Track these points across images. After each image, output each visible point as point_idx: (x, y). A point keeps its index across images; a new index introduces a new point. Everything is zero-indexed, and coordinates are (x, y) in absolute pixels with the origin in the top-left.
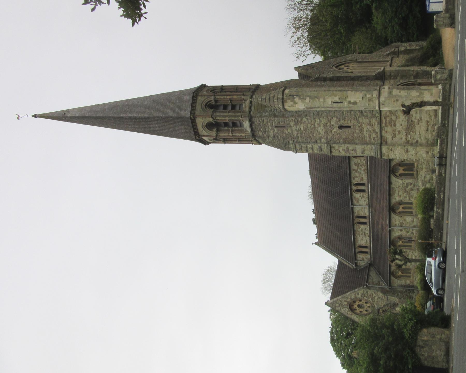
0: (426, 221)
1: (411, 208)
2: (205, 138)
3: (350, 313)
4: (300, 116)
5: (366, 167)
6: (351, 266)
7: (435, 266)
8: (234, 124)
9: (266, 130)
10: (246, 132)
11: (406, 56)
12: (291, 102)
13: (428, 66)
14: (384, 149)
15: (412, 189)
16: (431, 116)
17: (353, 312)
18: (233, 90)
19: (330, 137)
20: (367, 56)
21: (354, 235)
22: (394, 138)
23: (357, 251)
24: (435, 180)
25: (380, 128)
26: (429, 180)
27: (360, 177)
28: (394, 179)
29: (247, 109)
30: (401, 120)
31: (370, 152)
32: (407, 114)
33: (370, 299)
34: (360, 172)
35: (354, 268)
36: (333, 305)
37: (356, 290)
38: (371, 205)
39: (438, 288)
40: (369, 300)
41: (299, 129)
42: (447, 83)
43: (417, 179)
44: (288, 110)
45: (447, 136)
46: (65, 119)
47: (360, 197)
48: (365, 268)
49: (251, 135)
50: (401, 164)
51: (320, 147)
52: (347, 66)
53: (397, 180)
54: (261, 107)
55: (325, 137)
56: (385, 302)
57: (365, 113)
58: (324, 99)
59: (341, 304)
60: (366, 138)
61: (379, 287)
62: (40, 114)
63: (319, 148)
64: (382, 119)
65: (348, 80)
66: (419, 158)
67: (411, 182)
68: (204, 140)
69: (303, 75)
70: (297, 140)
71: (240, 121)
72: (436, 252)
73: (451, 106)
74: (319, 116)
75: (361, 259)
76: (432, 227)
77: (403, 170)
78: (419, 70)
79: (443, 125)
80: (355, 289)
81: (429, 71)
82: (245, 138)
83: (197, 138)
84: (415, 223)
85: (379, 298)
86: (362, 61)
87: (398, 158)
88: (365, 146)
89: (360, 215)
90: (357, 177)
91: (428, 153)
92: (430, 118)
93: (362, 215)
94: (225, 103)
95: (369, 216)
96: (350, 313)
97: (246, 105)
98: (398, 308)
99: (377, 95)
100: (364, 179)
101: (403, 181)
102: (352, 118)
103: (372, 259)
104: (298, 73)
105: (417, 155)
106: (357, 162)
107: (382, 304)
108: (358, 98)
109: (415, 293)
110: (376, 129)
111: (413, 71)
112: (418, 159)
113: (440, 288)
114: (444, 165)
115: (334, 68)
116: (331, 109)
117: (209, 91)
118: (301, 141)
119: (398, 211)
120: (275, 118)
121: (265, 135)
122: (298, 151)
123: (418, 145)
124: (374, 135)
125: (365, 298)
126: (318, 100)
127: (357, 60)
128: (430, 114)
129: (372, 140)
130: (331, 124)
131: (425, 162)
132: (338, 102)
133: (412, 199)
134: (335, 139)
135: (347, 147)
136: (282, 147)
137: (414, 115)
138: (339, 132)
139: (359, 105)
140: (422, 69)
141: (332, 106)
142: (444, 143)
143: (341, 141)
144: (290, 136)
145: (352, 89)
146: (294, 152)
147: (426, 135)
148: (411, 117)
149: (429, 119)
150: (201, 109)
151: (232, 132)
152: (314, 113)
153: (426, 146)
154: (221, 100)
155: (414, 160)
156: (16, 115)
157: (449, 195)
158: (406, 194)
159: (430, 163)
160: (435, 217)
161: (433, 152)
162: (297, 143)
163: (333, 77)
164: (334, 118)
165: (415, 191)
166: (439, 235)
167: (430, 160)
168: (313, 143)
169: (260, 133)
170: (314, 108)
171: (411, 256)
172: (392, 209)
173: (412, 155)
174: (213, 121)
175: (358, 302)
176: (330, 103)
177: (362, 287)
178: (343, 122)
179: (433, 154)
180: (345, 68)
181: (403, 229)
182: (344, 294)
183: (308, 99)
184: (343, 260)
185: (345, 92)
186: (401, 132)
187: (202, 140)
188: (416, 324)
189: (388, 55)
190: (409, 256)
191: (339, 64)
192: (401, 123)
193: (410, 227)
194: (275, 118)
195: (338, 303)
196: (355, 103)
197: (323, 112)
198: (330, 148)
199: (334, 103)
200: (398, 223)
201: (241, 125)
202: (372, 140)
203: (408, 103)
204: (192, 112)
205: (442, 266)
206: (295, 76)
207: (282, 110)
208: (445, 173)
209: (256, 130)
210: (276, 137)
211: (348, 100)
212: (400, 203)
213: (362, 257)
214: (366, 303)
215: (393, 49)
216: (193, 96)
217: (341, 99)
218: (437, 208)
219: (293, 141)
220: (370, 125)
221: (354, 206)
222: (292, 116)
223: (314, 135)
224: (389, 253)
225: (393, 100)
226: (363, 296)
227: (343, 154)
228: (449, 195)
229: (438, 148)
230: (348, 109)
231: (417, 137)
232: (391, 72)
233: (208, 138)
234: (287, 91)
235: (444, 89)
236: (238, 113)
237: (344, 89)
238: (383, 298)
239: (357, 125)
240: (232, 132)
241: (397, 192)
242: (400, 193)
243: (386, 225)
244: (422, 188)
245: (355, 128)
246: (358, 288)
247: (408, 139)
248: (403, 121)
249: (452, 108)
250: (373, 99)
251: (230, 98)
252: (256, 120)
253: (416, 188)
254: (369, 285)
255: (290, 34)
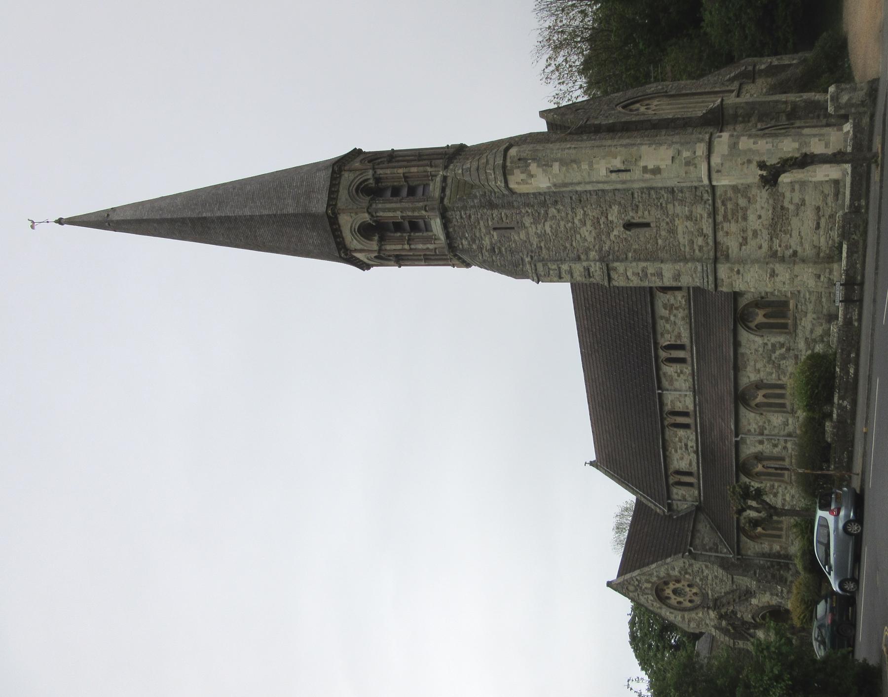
0: (814, 426)
1: (782, 396)
2: (360, 256)
3: (657, 604)
4: (544, 204)
5: (687, 311)
6: (660, 509)
7: (836, 528)
8: (414, 226)
9: (475, 236)
10: (436, 242)
11: (769, 80)
12: (522, 173)
13: (820, 92)
14: (723, 271)
15: (783, 357)
16: (826, 197)
17: (664, 604)
18: (413, 157)
19: (606, 248)
20: (685, 84)
21: (665, 449)
22: (744, 247)
23: (671, 480)
24: (836, 335)
25: (712, 225)
26: (822, 336)
27: (676, 333)
28: (745, 336)
29: (437, 194)
30: (758, 206)
31: (693, 278)
32: (771, 186)
33: (698, 580)
34: (674, 322)
35: (666, 514)
36: (623, 588)
37: (669, 560)
38: (698, 388)
39: (842, 578)
40: (696, 582)
41: (543, 231)
42: (865, 113)
43: (796, 335)
44: (518, 191)
45: (865, 232)
46: (109, 225)
47: (676, 372)
48: (687, 515)
49: (447, 248)
50: (761, 302)
51: (587, 270)
52: (647, 105)
53: (752, 337)
54: (465, 189)
55: (597, 247)
56: (728, 587)
57: (680, 194)
58: (591, 164)
59: (638, 585)
60: (682, 249)
61: (715, 556)
62: (67, 219)
63: (585, 272)
64: (716, 205)
65: (646, 129)
66: (799, 288)
67: (783, 342)
68: (358, 259)
69: (556, 125)
70: (540, 255)
71: (423, 218)
72: (838, 497)
73: (876, 162)
74: (582, 203)
75: (680, 498)
76: (829, 440)
77: (765, 316)
78: (797, 99)
79: (855, 210)
80: (666, 558)
81: (820, 101)
82: (435, 252)
83: (343, 255)
84: (790, 428)
85: (716, 577)
86: (677, 93)
87: (752, 290)
88: (682, 264)
89: (676, 410)
90: (668, 332)
91: (819, 277)
92: (823, 200)
93: (681, 410)
94: (395, 184)
95: (695, 411)
96: (658, 605)
97: (436, 186)
98: (755, 600)
99: (705, 152)
100: (683, 336)
101: (763, 340)
102: (651, 206)
103: (702, 498)
104: (547, 123)
105: (795, 282)
106: (668, 301)
107: (723, 591)
108: (662, 160)
109: (790, 569)
110: (704, 227)
111: (786, 102)
112: (796, 292)
113: (849, 577)
114: (857, 301)
115: (619, 109)
116: (606, 187)
117: (366, 162)
118: (546, 257)
119: (753, 403)
120: (492, 209)
121: (474, 247)
122: (541, 278)
123: (798, 261)
124: (700, 241)
125: (687, 576)
126: (578, 168)
127: (666, 92)
128: (823, 192)
129: (697, 251)
130: (608, 220)
131: (813, 299)
132: (619, 171)
133: (784, 377)
134: (618, 251)
135: (644, 267)
136: (510, 269)
137: (788, 195)
138: (625, 236)
139: (665, 174)
140: (804, 97)
141: (607, 179)
142: (857, 252)
143: (630, 255)
144: (525, 246)
145: (649, 140)
146: (533, 281)
147: (814, 238)
148: (781, 198)
149: (820, 203)
150: (347, 196)
151: (410, 241)
152: (571, 198)
153: (815, 263)
154: (387, 178)
155: (789, 295)
156: (29, 220)
157: (871, 369)
158: (771, 366)
159: (824, 300)
160: (835, 416)
161: (830, 275)
162: (539, 261)
163: (614, 124)
164: (613, 207)
165: (790, 360)
166: (845, 456)
167: (823, 293)
168: (572, 260)
169: (465, 242)
170: (572, 184)
171: (782, 496)
172: (741, 398)
173: (784, 283)
174: (371, 220)
175: (674, 585)
176: (603, 172)
177: (680, 555)
178: (634, 215)
179: (830, 279)
180: (643, 109)
181: (765, 440)
182: (646, 566)
183: (556, 166)
184: (644, 497)
185: (635, 148)
186: (759, 233)
187: (355, 260)
188: (791, 692)
189: (732, 80)
190: (779, 495)
191: (629, 101)
192: (758, 213)
193: (780, 436)
194: (492, 209)
195: (633, 585)
196: (657, 171)
197: (591, 195)
198: (608, 270)
199: (612, 172)
200: (753, 427)
201: (428, 228)
202: (697, 251)
203: (772, 161)
204: (331, 203)
205: (854, 528)
206: (541, 126)
207: (506, 192)
208: (860, 320)
209: (455, 236)
210: (496, 250)
211: (642, 163)
212: (759, 385)
213: (682, 494)
214: (689, 586)
215: (744, 68)
216: (333, 172)
217: (626, 163)
218: (839, 398)
219: (532, 257)
220: (692, 219)
221: (664, 392)
222: (528, 205)
223: (574, 244)
224: (732, 494)
225: (739, 161)
226: (683, 572)
227: (635, 282)
228: (871, 369)
229: (844, 262)
230: (643, 185)
231: (794, 242)
232: (736, 107)
233: (364, 254)
234: (513, 152)
235: (857, 127)
236: (419, 202)
237: (633, 142)
238: (725, 578)
239: (663, 220)
240: (410, 242)
241: (752, 363)
242: (759, 365)
243: (729, 431)
244: (805, 354)
245: (658, 227)
246: (672, 557)
247: (774, 248)
248: (762, 208)
249: (877, 166)
250: (696, 161)
251: (404, 174)
252: (455, 217)
253: (792, 353)
254: (696, 552)
255: (543, 63)
